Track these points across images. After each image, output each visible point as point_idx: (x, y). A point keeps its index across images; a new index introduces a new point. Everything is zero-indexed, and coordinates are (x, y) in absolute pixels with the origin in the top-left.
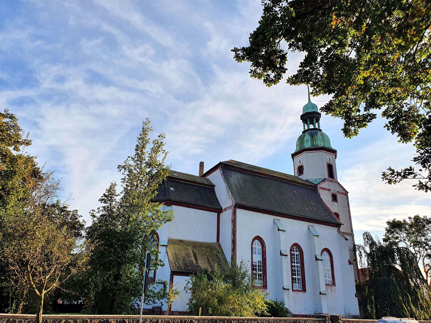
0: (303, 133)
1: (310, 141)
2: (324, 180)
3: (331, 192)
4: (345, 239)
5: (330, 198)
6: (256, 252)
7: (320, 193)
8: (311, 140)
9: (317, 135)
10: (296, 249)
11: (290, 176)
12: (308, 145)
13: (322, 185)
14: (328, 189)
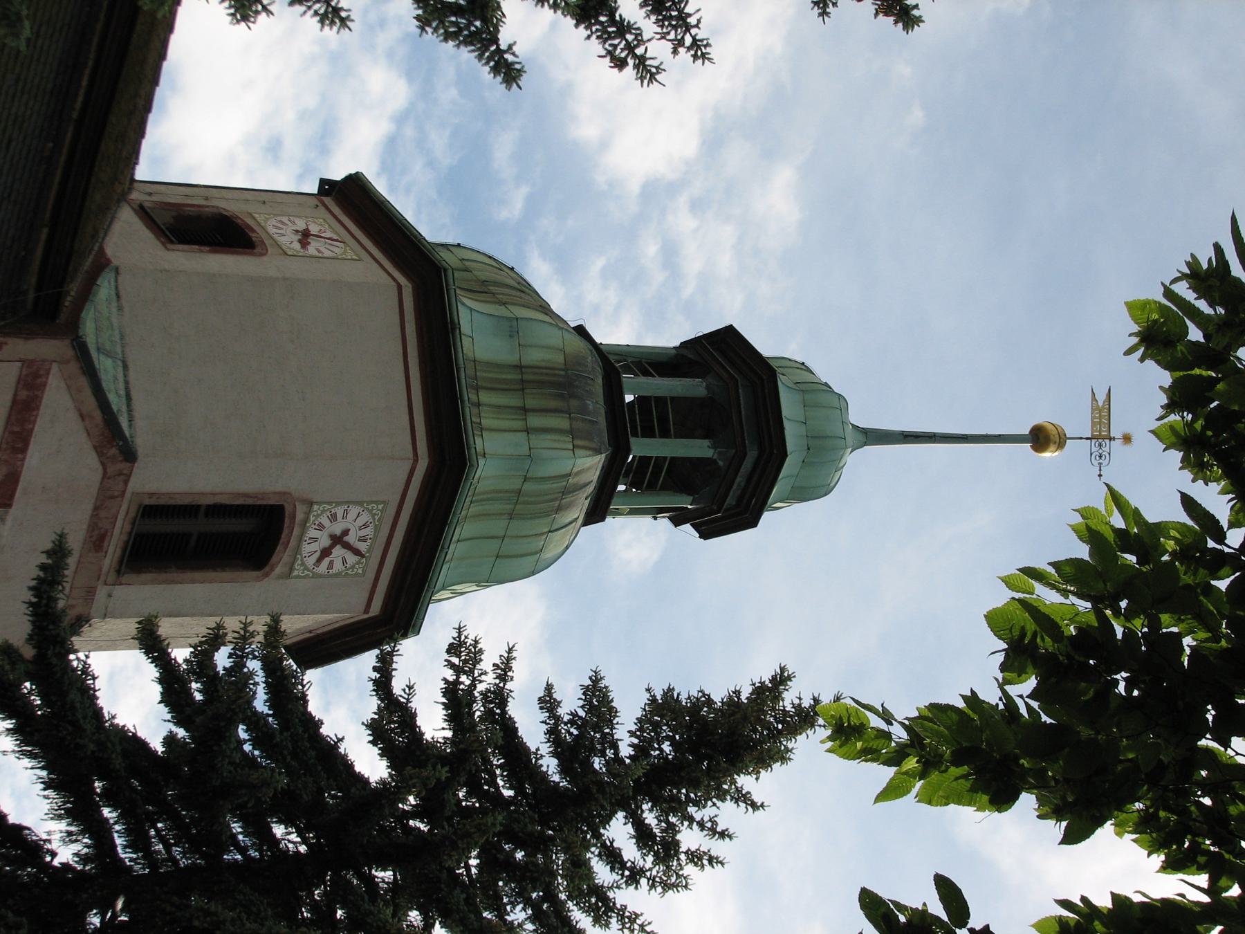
0: (575, 328)
8: (519, 367)
9: (572, 433)
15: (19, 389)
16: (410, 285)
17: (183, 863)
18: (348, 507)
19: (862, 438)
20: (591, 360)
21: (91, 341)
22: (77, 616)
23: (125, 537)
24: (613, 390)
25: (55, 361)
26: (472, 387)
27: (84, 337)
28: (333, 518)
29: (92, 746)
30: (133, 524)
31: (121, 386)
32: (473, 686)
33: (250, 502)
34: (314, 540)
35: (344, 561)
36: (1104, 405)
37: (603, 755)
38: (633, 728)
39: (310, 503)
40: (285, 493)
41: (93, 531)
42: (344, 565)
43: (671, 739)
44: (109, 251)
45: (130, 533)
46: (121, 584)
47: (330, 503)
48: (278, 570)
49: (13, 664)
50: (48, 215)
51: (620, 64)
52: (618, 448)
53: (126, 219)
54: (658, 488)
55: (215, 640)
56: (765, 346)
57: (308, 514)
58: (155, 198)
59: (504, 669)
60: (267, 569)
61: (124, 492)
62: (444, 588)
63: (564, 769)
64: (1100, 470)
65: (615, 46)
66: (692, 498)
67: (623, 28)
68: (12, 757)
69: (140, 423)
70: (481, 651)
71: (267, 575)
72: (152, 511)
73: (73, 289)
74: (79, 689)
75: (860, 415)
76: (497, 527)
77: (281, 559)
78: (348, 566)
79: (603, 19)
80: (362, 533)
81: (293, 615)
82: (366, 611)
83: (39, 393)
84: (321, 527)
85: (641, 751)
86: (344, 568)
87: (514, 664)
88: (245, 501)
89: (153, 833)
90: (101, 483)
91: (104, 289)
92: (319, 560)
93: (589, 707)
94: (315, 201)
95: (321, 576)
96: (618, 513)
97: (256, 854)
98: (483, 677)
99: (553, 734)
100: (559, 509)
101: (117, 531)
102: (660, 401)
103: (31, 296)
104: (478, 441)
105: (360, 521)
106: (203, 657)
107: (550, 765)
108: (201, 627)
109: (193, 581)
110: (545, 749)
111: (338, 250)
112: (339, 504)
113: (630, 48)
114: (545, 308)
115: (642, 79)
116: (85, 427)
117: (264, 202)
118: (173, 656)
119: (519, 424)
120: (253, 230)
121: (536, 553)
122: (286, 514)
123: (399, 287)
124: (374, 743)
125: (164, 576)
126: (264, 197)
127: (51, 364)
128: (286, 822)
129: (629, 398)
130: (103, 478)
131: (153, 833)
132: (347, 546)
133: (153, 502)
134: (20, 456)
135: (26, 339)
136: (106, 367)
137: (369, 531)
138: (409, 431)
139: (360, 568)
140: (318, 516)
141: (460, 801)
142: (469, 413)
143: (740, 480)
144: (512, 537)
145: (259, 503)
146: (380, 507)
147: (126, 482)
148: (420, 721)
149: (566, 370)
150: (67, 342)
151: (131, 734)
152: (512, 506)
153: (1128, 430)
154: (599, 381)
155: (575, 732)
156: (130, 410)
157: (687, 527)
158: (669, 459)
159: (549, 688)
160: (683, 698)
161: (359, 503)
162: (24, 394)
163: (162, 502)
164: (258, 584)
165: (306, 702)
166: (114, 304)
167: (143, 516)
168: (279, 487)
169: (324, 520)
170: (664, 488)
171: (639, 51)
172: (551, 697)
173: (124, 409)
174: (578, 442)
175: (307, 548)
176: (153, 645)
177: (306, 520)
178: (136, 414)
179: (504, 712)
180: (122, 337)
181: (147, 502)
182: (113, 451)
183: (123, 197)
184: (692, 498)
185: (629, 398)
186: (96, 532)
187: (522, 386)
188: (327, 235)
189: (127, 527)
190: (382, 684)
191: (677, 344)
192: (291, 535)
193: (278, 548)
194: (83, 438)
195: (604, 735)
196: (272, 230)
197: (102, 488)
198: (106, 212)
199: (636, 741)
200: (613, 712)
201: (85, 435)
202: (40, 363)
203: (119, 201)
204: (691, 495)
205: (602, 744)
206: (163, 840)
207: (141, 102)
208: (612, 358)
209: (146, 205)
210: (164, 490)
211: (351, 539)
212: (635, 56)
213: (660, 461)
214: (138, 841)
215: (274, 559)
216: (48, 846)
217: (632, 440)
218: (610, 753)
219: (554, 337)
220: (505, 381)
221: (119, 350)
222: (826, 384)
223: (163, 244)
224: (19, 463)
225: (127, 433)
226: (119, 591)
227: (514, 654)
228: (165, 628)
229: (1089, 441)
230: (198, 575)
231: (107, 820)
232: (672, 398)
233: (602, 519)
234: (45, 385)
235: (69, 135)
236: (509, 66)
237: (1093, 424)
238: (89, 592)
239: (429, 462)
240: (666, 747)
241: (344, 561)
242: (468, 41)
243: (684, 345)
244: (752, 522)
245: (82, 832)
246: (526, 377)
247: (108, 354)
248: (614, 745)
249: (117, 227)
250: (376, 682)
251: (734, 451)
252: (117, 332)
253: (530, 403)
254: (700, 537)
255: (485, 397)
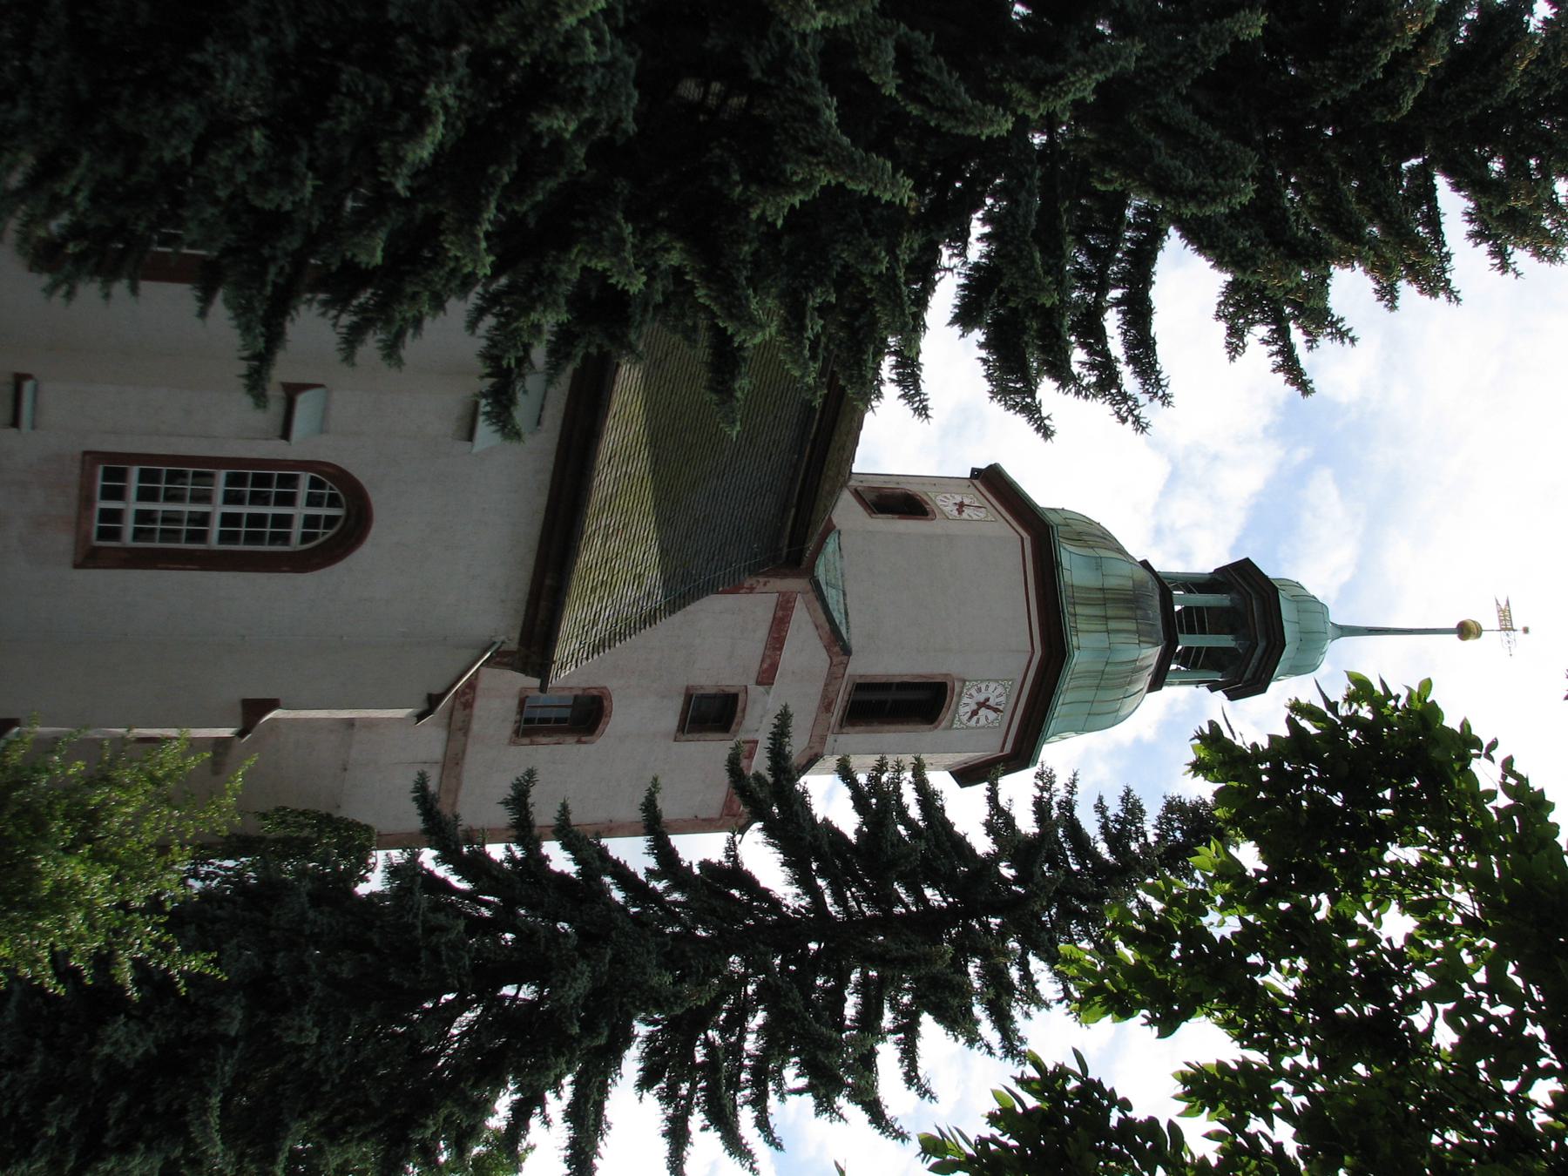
0: (1141, 563)
1: (1098, 584)
2: (837, 643)
3: (752, 687)
4: (437, 690)
5: (712, 675)
6: (275, 516)
7: (751, 590)
8: (1102, 590)
9: (1138, 632)
10: (330, 521)
11: (851, 458)
12: (1074, 568)
13: (802, 621)
14: (774, 667)
17: (868, 913)
19: (1339, 632)
20: (1152, 584)
21: (822, 579)
23: (844, 704)
24: (1167, 601)
26: (1070, 603)
28: (979, 690)
29: (809, 838)
31: (842, 606)
32: (1051, 798)
33: (924, 680)
34: (967, 704)
35: (987, 718)
37: (1138, 841)
38: (1155, 823)
39: (964, 681)
40: (947, 675)
43: (1180, 829)
44: (835, 520)
47: (976, 681)
48: (943, 724)
49: (761, 786)
50: (795, 501)
51: (1124, 420)
52: (1171, 642)
53: (846, 501)
55: (881, 768)
56: (1270, 571)
57: (962, 688)
58: (865, 484)
59: (1072, 787)
60: (936, 723)
62: (1053, 735)
63: (1112, 851)
65: (1121, 409)
67: (1125, 397)
68: (761, 845)
69: (853, 630)
70: (1054, 776)
71: (936, 728)
72: (862, 687)
73: (811, 546)
74: (801, 804)
75: (1338, 617)
76: (1089, 695)
77: (945, 720)
79: (1113, 391)
80: (998, 700)
82: (1002, 751)
84: (971, 696)
85: (1161, 837)
87: (1078, 784)
89: (849, 894)
91: (831, 545)
92: (970, 718)
93: (1127, 811)
94: (967, 483)
95: (973, 728)
96: (1171, 684)
97: (914, 909)
98: (1057, 793)
99: (1104, 828)
100: (1130, 683)
101: (839, 699)
102: (1199, 609)
103: (785, 550)
104: (1074, 639)
105: (997, 693)
106: (874, 780)
107: (1102, 848)
108: (872, 760)
109: (889, 732)
110: (1099, 837)
111: (982, 514)
112: (982, 681)
113: (1130, 411)
114: (1120, 550)
115: (1137, 430)
119: (1103, 628)
120: (927, 504)
123: (1022, 538)
124: (988, 835)
125: (869, 728)
126: (935, 481)
128: (934, 886)
129: (1177, 608)
131: (849, 894)
132: (989, 707)
133: (862, 681)
136: (832, 595)
137: (1002, 699)
140: (968, 689)
141: (1044, 872)
142: (1068, 621)
143: (1254, 662)
148: (1017, 822)
149: (1134, 591)
150: (807, 580)
151: (1516, 963)
152: (1097, 682)
154: (1158, 597)
155: (1119, 827)
156: (847, 622)
157: (1220, 693)
159: (1101, 799)
160: (1187, 801)
161: (996, 681)
162: (780, 614)
163: (868, 680)
165: (944, 811)
166: (838, 554)
167: (856, 690)
168: (944, 671)
169: (973, 692)
170: (1203, 667)
171: (1136, 413)
172: (1101, 803)
173: (844, 621)
174: (1142, 639)
175: (962, 710)
176: (846, 774)
177: (961, 692)
178: (851, 625)
179: (1072, 815)
180: (842, 576)
181: (858, 681)
182: (837, 649)
183: (844, 484)
185: (1177, 608)
187: (1104, 602)
188: (977, 504)
189: (846, 698)
190: (993, 799)
191: (1212, 571)
194: (818, 641)
195: (1137, 828)
196: (939, 503)
198: (833, 495)
199: (1158, 831)
200: (1142, 812)
203: (842, 487)
205: (1136, 834)
206: (855, 898)
207: (855, 425)
208: (1166, 581)
209: (859, 489)
210: (869, 673)
211: (991, 703)
212: (1133, 415)
213: (1199, 649)
214: (840, 899)
215: (941, 717)
216: (784, 902)
217: (1180, 636)
218: (1141, 840)
219: (1126, 569)
220: (1093, 599)
221: (840, 584)
222: (1313, 597)
223: (870, 515)
225: (845, 638)
226: (841, 738)
227: (1078, 777)
228: (855, 762)
230: (893, 727)
231: (820, 887)
232: (1208, 608)
233: (1160, 688)
235: (808, 450)
236: (1046, 428)
237: (1501, 621)
240: (1178, 834)
241: (987, 718)
242: (1022, 410)
243: (1218, 571)
244: (1263, 689)
245: (804, 894)
246: (1107, 596)
247: (833, 587)
248: (1144, 835)
249: (840, 504)
250: (988, 798)
252: (839, 572)
253: (1110, 613)
255: (1079, 610)
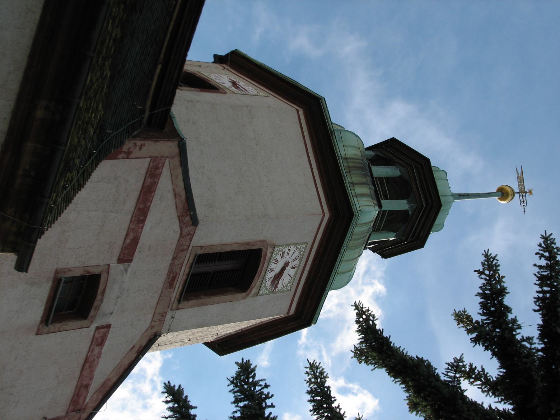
15: (147, 178)
16: (302, 110)
18: (290, 247)
22: (155, 333)
23: (185, 277)
25: (168, 157)
27: (185, 139)
30: (191, 268)
34: (272, 270)
36: (521, 176)
39: (274, 247)
41: (170, 275)
42: (283, 285)
45: (188, 274)
46: (179, 309)
48: (254, 291)
54: (381, 230)
60: (249, 291)
61: (189, 246)
64: (524, 208)
66: (395, 234)
71: (248, 295)
78: (285, 285)
81: (256, 319)
82: (288, 313)
83: (156, 180)
86: (283, 287)
88: (245, 247)
90: (178, 241)
101: (182, 273)
116: (176, 202)
117: (200, 66)
118: (517, 338)
121: (349, 271)
122: (263, 255)
123: (297, 110)
127: (166, 159)
130: (180, 238)
134: (141, 225)
135: (156, 141)
137: (297, 262)
138: (317, 197)
139: (289, 286)
144: (347, 261)
145: (252, 248)
146: (304, 246)
147: (191, 239)
153: (530, 189)
158: (387, 212)
161: (295, 244)
164: (242, 301)
168: (262, 238)
181: (200, 252)
182: (188, 219)
184: (395, 234)
186: (172, 275)
189: (187, 270)
192: (263, 268)
193: (255, 277)
197: (179, 245)
201: (175, 208)
202: (160, 158)
204: (395, 232)
210: (208, 244)
224: (140, 230)
229: (518, 194)
230: (216, 298)
234: (160, 174)
238: (163, 316)
239: (329, 216)
246: (351, 164)
251: (417, 205)
254: (382, 258)
